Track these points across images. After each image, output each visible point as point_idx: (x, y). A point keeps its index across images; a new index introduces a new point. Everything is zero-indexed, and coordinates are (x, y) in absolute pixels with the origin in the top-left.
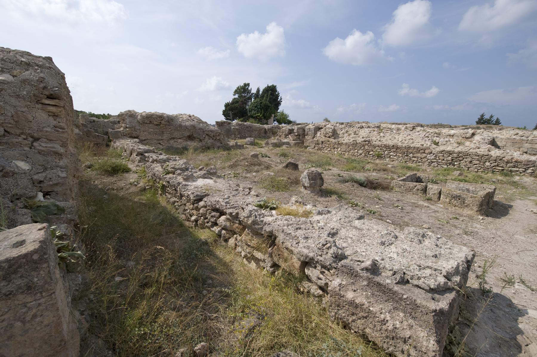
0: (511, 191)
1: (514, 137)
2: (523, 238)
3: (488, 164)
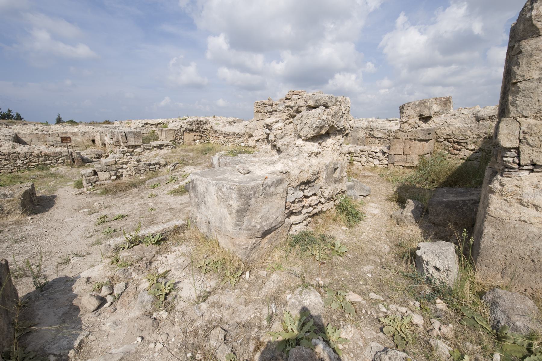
0: (52, 182)
1: (36, 132)
2: (71, 219)
3: (19, 162)
